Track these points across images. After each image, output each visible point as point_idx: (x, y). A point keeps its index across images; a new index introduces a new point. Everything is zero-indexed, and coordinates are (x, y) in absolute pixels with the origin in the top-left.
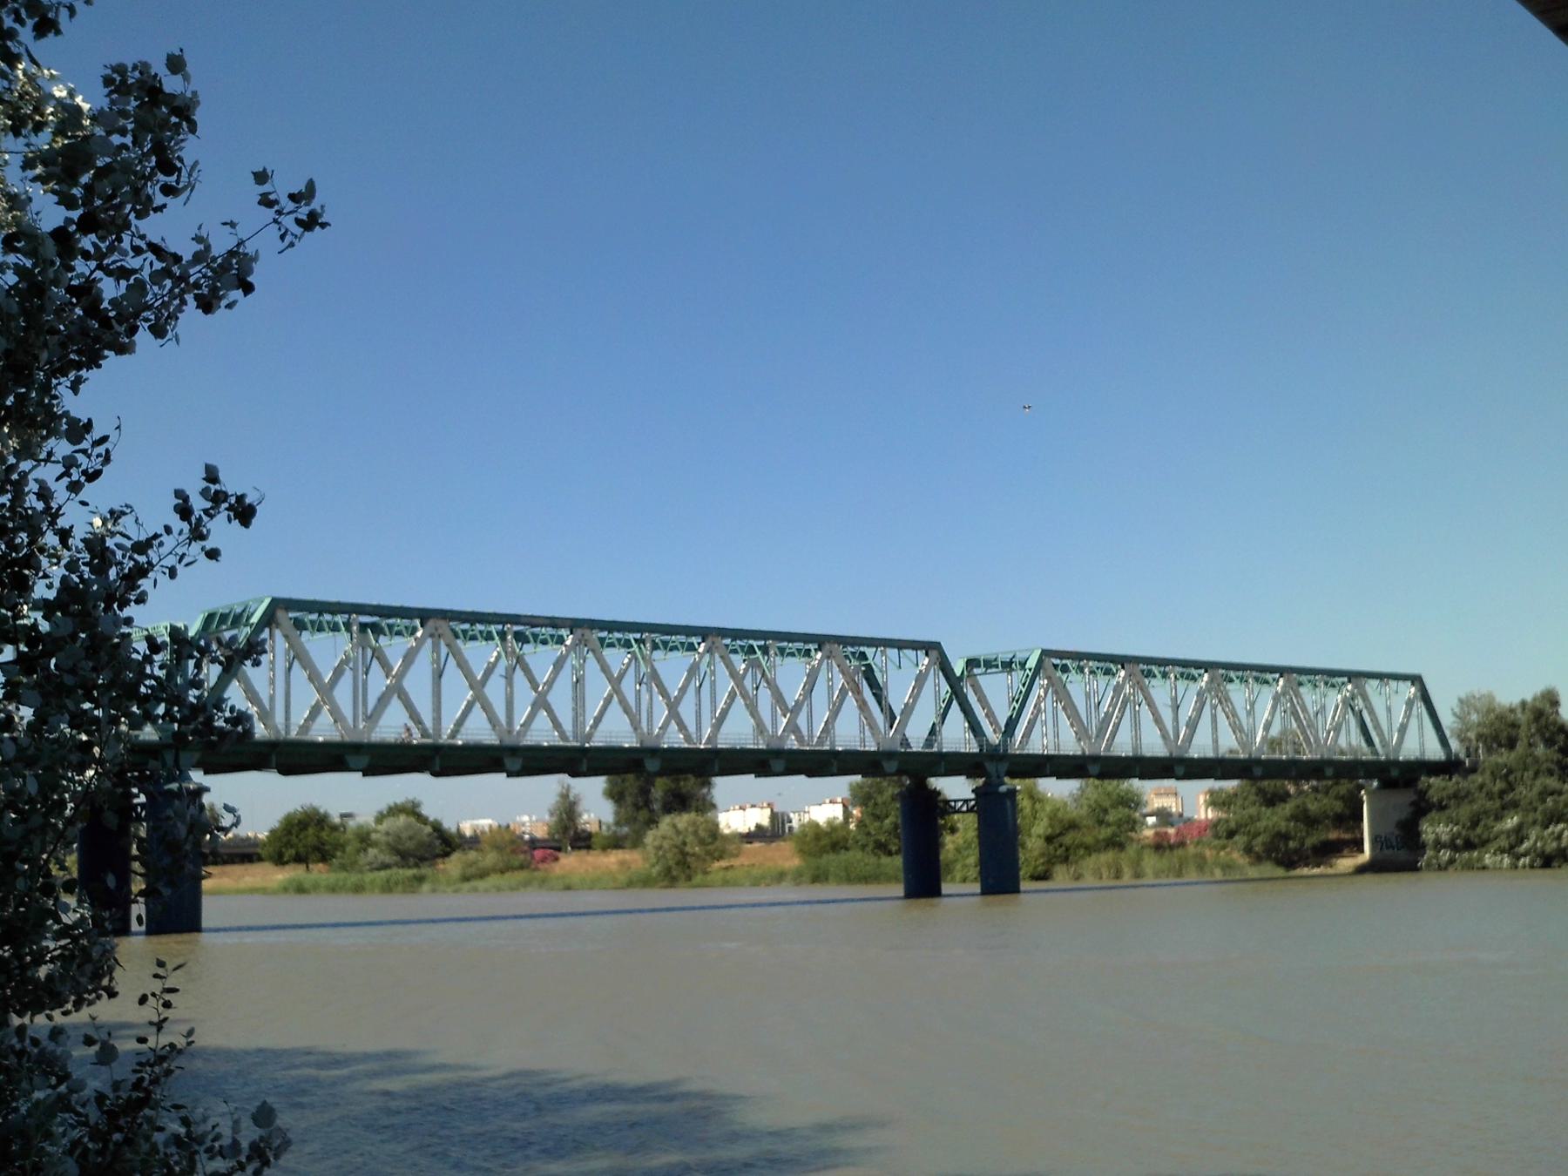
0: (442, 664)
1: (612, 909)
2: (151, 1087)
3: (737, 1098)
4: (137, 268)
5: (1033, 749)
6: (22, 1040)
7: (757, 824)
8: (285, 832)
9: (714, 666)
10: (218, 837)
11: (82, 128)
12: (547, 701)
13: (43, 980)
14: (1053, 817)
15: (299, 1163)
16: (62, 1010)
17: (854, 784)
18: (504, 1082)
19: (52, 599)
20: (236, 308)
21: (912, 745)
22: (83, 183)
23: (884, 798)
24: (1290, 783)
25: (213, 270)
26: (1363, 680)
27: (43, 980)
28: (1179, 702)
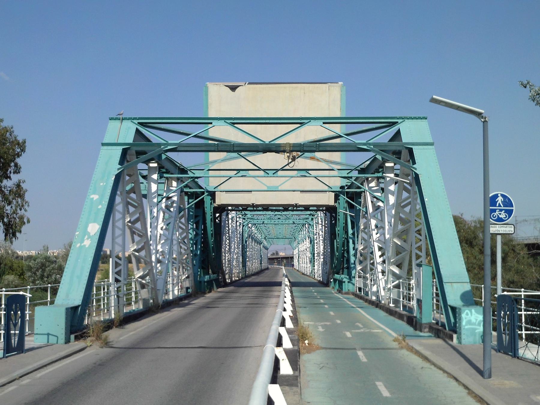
13: (376, 382)
18: (211, 306)
27: (376, 382)
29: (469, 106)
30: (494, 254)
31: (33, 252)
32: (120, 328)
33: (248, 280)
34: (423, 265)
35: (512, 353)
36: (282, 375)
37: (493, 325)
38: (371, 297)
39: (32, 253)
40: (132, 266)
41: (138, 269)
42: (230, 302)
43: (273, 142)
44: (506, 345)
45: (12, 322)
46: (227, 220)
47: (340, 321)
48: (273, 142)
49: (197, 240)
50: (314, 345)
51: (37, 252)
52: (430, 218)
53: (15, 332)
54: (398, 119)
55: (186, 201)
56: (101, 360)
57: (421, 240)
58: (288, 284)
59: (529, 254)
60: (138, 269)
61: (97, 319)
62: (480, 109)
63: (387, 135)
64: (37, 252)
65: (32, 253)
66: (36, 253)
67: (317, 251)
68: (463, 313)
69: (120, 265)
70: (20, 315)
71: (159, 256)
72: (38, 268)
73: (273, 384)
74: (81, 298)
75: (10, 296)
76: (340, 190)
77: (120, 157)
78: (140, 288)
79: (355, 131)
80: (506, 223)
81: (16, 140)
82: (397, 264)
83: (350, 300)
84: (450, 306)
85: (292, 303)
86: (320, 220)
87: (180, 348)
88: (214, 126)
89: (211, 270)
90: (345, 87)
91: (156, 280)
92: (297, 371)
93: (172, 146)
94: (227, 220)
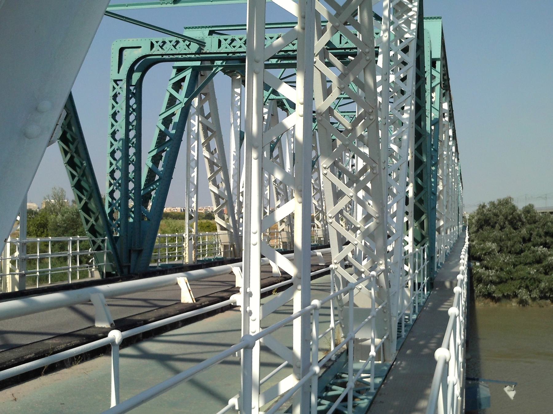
13: (381, 67)
27: (111, 407)
31: (178, 208)
39: (177, 210)
40: (330, 250)
41: (278, 200)
43: (74, 333)
48: (74, 333)
49: (420, 270)
51: (182, 209)
57: (403, 92)
60: (278, 200)
61: (115, 235)
64: (182, 209)
65: (177, 210)
66: (181, 209)
67: (240, 47)
70: (365, 174)
71: (392, 205)
72: (66, 228)
73: (263, 298)
76: (273, 180)
77: (327, 4)
82: (177, 285)
84: (215, 177)
94: (345, 51)
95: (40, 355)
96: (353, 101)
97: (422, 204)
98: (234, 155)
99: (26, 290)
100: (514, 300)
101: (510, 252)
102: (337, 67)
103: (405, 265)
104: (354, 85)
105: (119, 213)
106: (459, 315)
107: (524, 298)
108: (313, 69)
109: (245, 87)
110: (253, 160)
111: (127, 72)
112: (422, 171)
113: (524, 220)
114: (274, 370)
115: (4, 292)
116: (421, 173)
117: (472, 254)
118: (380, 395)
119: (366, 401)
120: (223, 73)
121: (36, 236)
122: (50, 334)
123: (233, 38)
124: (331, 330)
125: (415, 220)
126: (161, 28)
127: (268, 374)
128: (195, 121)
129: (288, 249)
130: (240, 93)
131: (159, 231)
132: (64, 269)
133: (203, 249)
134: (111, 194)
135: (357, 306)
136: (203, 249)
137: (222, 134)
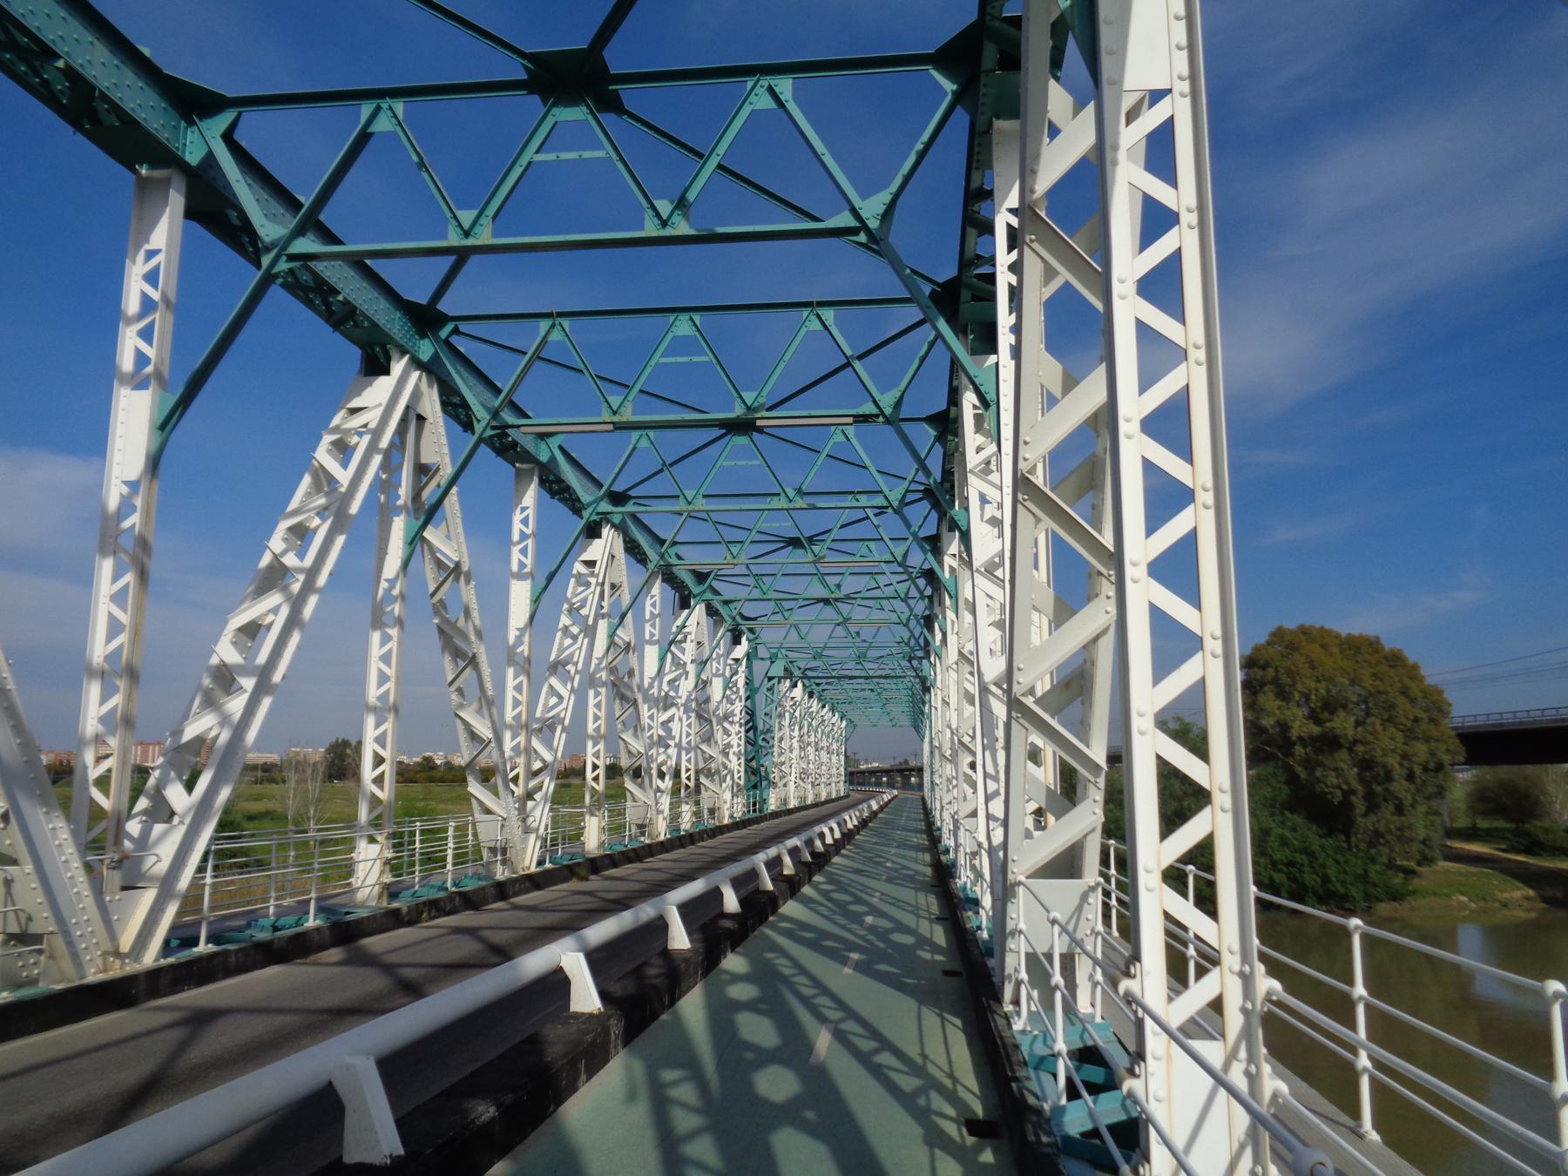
0: (280, 1020)
1: (1034, 255)
2: (1459, 785)
3: (993, 200)
4: (943, 406)
5: (979, 145)
6: (781, 778)
7: (330, 1084)
8: (960, 336)
9: (877, 891)
10: (274, 914)
11: (66, 873)
12: (1016, 216)
13: (945, 945)
14: (219, 859)
15: (401, 875)
16: (1106, 871)
17: (992, 973)
19: (395, 518)
20: (1131, 441)
21: (339, 286)
22: (723, 891)
23: (1273, 825)
24: (1473, 776)
25: (502, 443)
26: (172, 399)
27: (945, 945)
28: (565, 893)
29: (1401, 1085)
30: (327, 830)
32: (276, 1112)
33: (850, 888)
34: (674, 537)
35: (212, 908)
36: (393, 521)
37: (1248, 775)
38: (1037, 1136)
42: (722, 851)
44: (422, 547)
45: (829, 1008)
46: (788, 1114)
47: (341, 534)
50: (1349, 652)
52: (1108, 23)
53: (91, 672)
54: (1130, 930)
55: (559, 154)
56: (224, 187)
58: (982, 912)
59: (1049, 956)
62: (1408, 1089)
63: (994, 468)
66: (1156, 96)
68: (446, 423)
69: (1210, 959)
73: (1055, 137)
74: (928, 465)
75: (448, 379)
78: (410, 498)
79: (849, 543)
80: (688, 410)
81: (305, 759)
83: (1279, 1146)
85: (1013, 343)
86: (861, 694)
87: (1043, 906)
88: (988, 595)
89: (879, 963)
90: (389, 1161)
91: (280, 909)
92: (114, 736)
93: (934, 79)
95: (815, 705)
96: (1044, 533)
97: (65, 763)
98: (1009, 226)
99: (1382, 1138)
100: (1392, 789)
101: (929, 621)
102: (1085, 836)
103: (1016, 226)
104: (1355, 895)
105: (569, 594)
106: (1048, 1030)
107: (1272, 723)
108: (1030, 632)
109: (975, 792)
110: (919, 142)
111: (547, 1121)
112: (89, 829)
113: (1278, 785)
114: (1097, 298)
115: (78, 983)
116: (1093, 159)
117: (731, 816)
118: (1152, 1074)
119: (192, 1056)
120: (331, 329)
121: (1064, 951)
122: (1071, 917)
123: (843, 778)
124: (1099, 306)
125: (397, 1157)
126: (480, 368)
127: (1425, 1071)
128: (1142, 390)
129: (922, 826)
130: (988, 780)
131: (1023, 699)
132: (427, 847)
133: (274, 848)
134: (392, 582)
135: (1169, 996)
136: (274, 848)
137: (1078, 982)
